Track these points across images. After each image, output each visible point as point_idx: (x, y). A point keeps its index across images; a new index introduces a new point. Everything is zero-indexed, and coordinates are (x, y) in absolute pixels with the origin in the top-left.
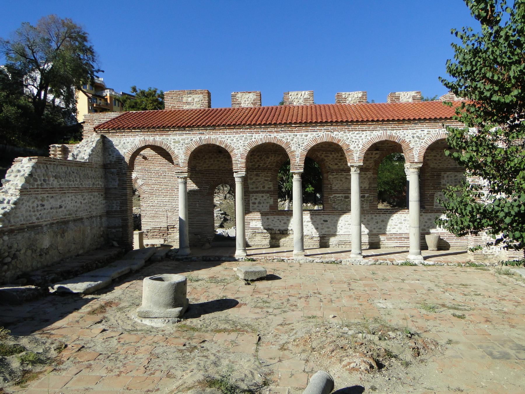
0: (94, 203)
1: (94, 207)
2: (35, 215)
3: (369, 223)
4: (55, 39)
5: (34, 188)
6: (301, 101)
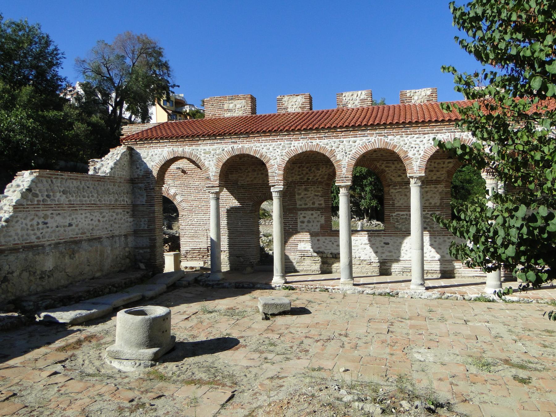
0: (117, 221)
1: (117, 226)
2: (35, 234)
3: (441, 247)
4: (131, 55)
5: (33, 205)
6: (356, 103)
